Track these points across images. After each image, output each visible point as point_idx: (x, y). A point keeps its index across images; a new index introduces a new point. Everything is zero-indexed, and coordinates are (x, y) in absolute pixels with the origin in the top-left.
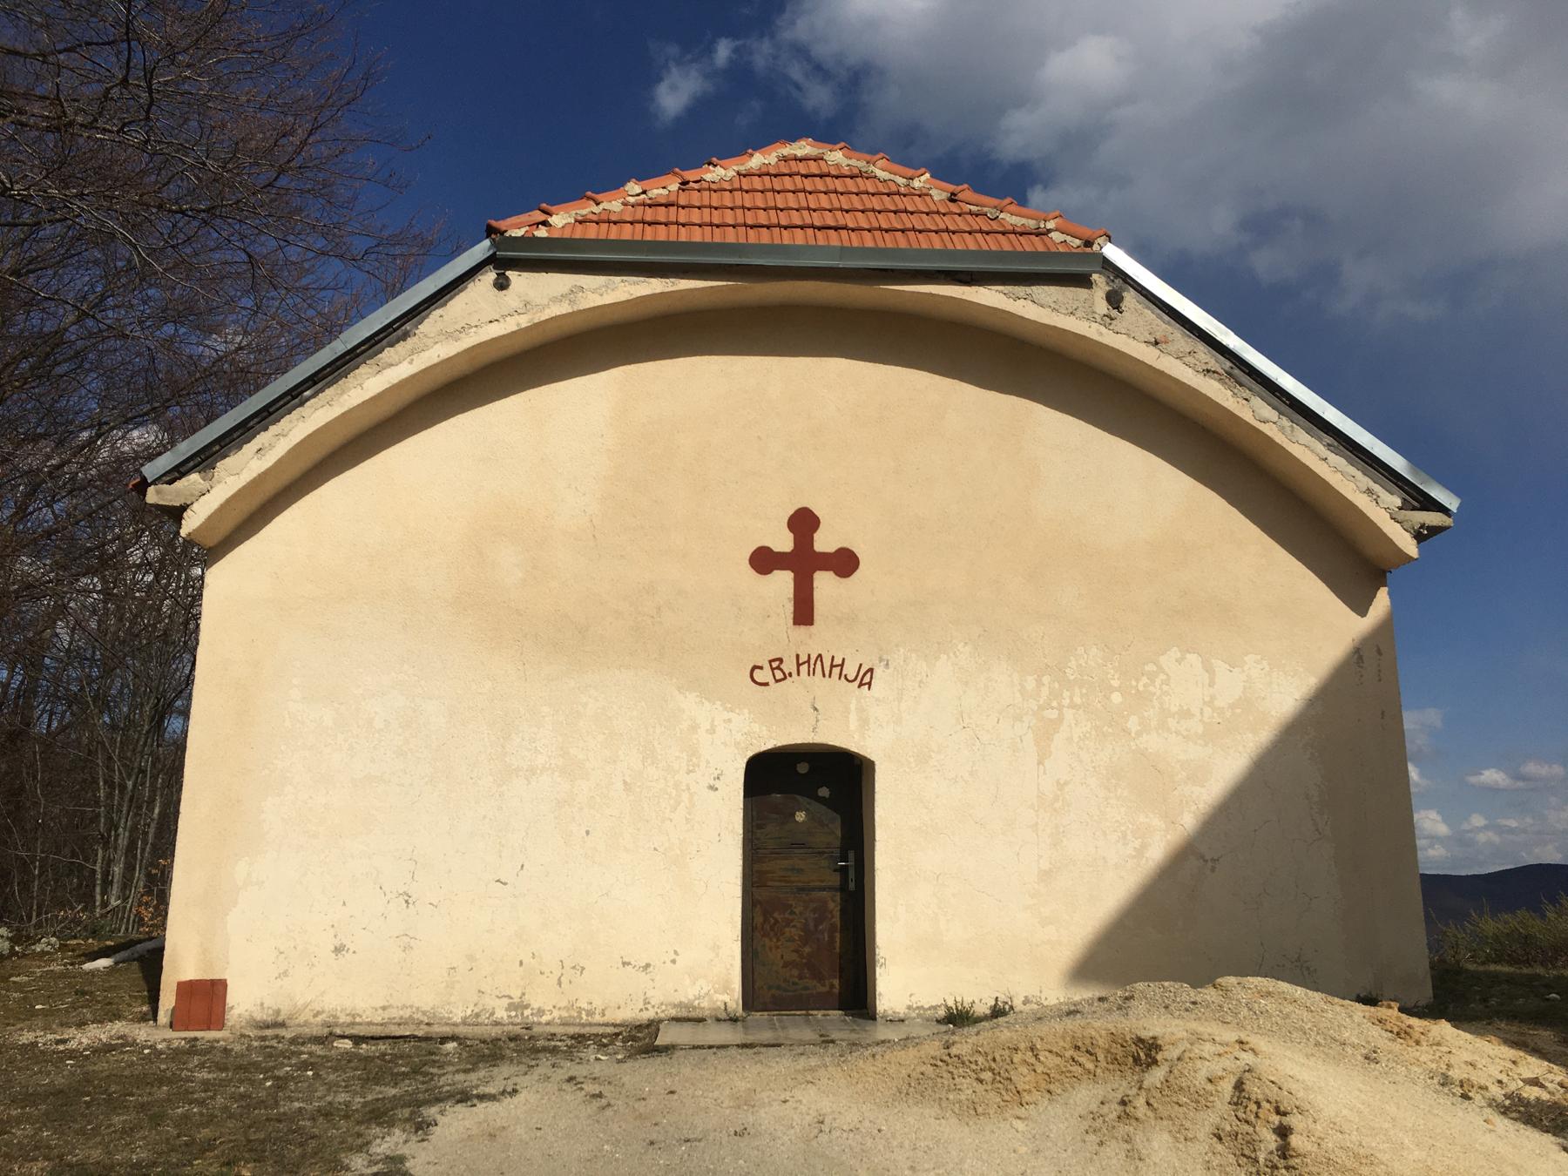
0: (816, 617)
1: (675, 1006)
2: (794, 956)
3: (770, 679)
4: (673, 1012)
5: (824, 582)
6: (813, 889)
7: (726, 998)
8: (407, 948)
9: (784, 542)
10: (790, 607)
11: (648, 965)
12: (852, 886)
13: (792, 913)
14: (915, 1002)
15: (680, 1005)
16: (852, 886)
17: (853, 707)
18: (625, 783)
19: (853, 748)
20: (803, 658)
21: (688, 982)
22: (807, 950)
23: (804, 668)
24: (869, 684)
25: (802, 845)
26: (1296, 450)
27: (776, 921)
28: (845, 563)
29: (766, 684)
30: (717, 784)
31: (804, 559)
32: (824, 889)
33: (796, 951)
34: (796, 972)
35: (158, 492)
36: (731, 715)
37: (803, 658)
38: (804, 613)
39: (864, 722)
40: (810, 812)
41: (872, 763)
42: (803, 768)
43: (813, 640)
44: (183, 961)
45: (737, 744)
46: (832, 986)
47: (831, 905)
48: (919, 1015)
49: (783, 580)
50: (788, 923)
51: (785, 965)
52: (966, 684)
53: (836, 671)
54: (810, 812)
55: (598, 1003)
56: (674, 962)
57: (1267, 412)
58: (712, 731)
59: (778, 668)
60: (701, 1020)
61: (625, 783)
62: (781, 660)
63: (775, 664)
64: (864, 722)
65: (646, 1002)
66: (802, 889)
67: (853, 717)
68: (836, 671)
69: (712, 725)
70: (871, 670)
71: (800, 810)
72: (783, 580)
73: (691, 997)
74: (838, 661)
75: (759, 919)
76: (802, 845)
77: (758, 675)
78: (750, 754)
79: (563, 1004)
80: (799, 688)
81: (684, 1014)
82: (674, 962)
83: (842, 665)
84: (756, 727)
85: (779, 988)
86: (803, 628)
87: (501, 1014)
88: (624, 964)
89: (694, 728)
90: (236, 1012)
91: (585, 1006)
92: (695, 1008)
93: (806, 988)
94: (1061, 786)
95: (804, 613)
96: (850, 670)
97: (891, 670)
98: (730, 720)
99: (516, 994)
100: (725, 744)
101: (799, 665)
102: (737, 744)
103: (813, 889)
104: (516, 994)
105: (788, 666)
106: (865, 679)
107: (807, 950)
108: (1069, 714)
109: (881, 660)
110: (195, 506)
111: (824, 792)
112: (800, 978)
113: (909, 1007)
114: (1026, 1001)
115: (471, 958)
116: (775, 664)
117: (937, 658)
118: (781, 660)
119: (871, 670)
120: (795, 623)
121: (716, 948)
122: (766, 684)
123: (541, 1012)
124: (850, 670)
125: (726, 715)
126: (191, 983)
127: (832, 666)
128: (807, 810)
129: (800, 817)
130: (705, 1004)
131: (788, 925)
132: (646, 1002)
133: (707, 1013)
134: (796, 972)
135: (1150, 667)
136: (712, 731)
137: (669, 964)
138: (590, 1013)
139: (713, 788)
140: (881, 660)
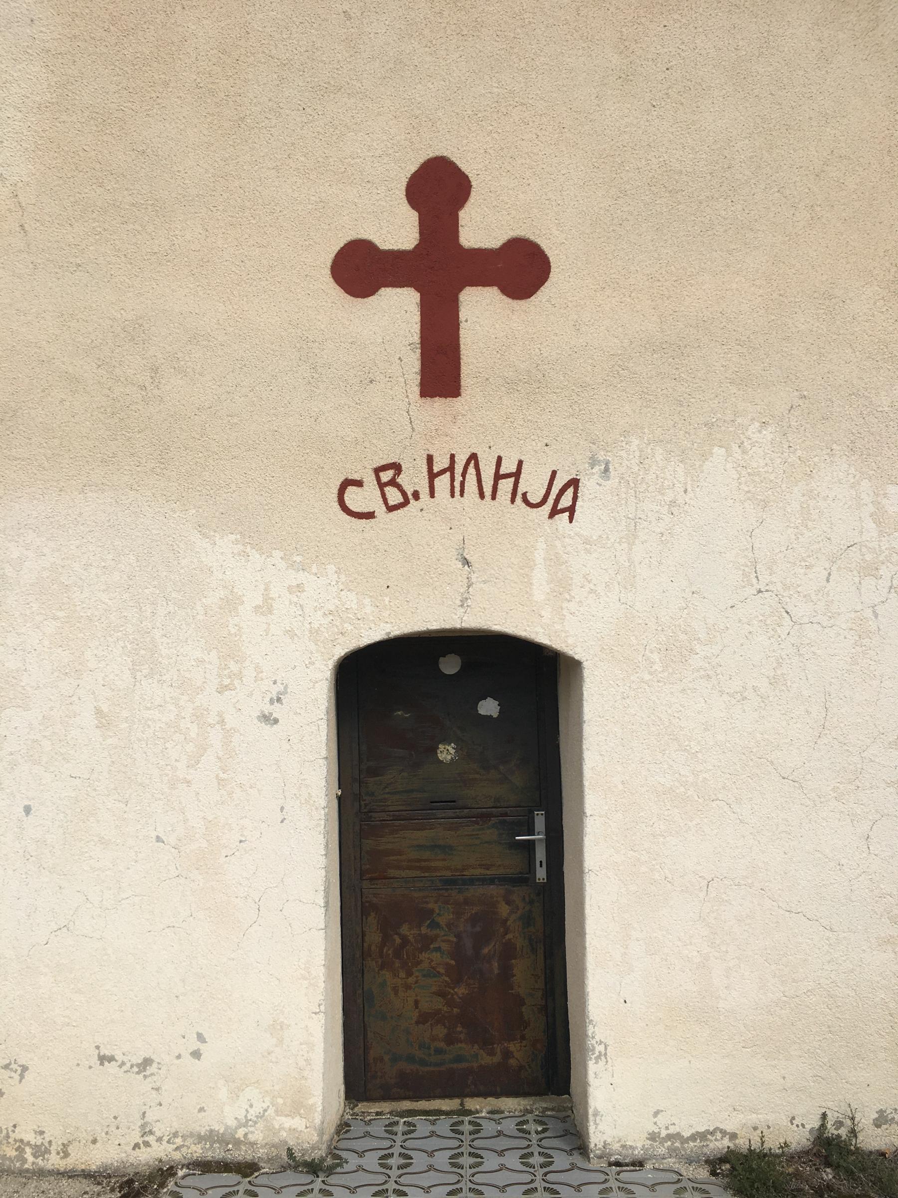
0: (462, 390)
1: (200, 1138)
2: (438, 1004)
3: (379, 508)
4: (197, 1151)
5: (481, 311)
6: (472, 881)
7: (298, 1123)
9: (399, 230)
10: (413, 362)
11: (147, 1062)
12: (541, 874)
13: (434, 925)
14: (666, 1124)
15: (211, 1137)
16: (541, 874)
17: (539, 556)
18: (98, 712)
19: (542, 639)
20: (440, 463)
21: (223, 1093)
22: (461, 991)
23: (442, 483)
24: (571, 510)
25: (450, 803)
27: (405, 941)
28: (521, 269)
29: (370, 515)
30: (277, 711)
31: (441, 262)
32: (492, 881)
33: (441, 994)
34: (440, 1031)
36: (302, 577)
37: (440, 463)
38: (440, 372)
39: (561, 587)
40: (455, 755)
41: (575, 666)
42: (450, 666)
43: (470, 424)
45: (315, 633)
46: (507, 1054)
47: (504, 910)
48: (672, 1152)
49: (398, 311)
50: (426, 943)
51: (423, 1019)
52: (765, 505)
53: (506, 485)
54: (455, 755)
55: (55, 1134)
56: (196, 1054)
58: (265, 608)
59: (393, 483)
60: (247, 1169)
61: (98, 712)
62: (397, 468)
63: (386, 476)
64: (561, 587)
65: (146, 1131)
66: (450, 882)
67: (540, 575)
68: (506, 485)
69: (267, 598)
70: (574, 483)
71: (446, 741)
72: (398, 311)
73: (232, 1123)
74: (508, 467)
75: (374, 937)
76: (450, 803)
77: (353, 497)
78: (341, 651)
80: (437, 521)
81: (216, 1153)
82: (196, 1054)
83: (517, 475)
84: (351, 600)
85: (411, 1059)
86: (439, 402)
89: (231, 603)
91: (30, 1137)
92: (237, 1143)
93: (459, 1059)
95: (440, 372)
96: (533, 484)
97: (613, 482)
98: (300, 587)
100: (290, 633)
101: (432, 476)
102: (315, 633)
103: (472, 881)
105: (413, 478)
106: (562, 499)
107: (461, 991)
109: (593, 462)
111: (489, 707)
112: (450, 1040)
113: (653, 1137)
114: (881, 1120)
116: (386, 476)
117: (705, 456)
118: (397, 468)
119: (574, 483)
120: (424, 394)
122: (370, 515)
124: (533, 484)
125: (294, 578)
126: (423, 385)
127: (498, 477)
128: (458, 741)
129: (446, 753)
130: (257, 1135)
131: (425, 948)
132: (146, 1131)
133: (261, 1152)
134: (440, 1031)
136: (265, 608)
137: (187, 1059)
138: (40, 1151)
139: (268, 719)
140: (593, 462)
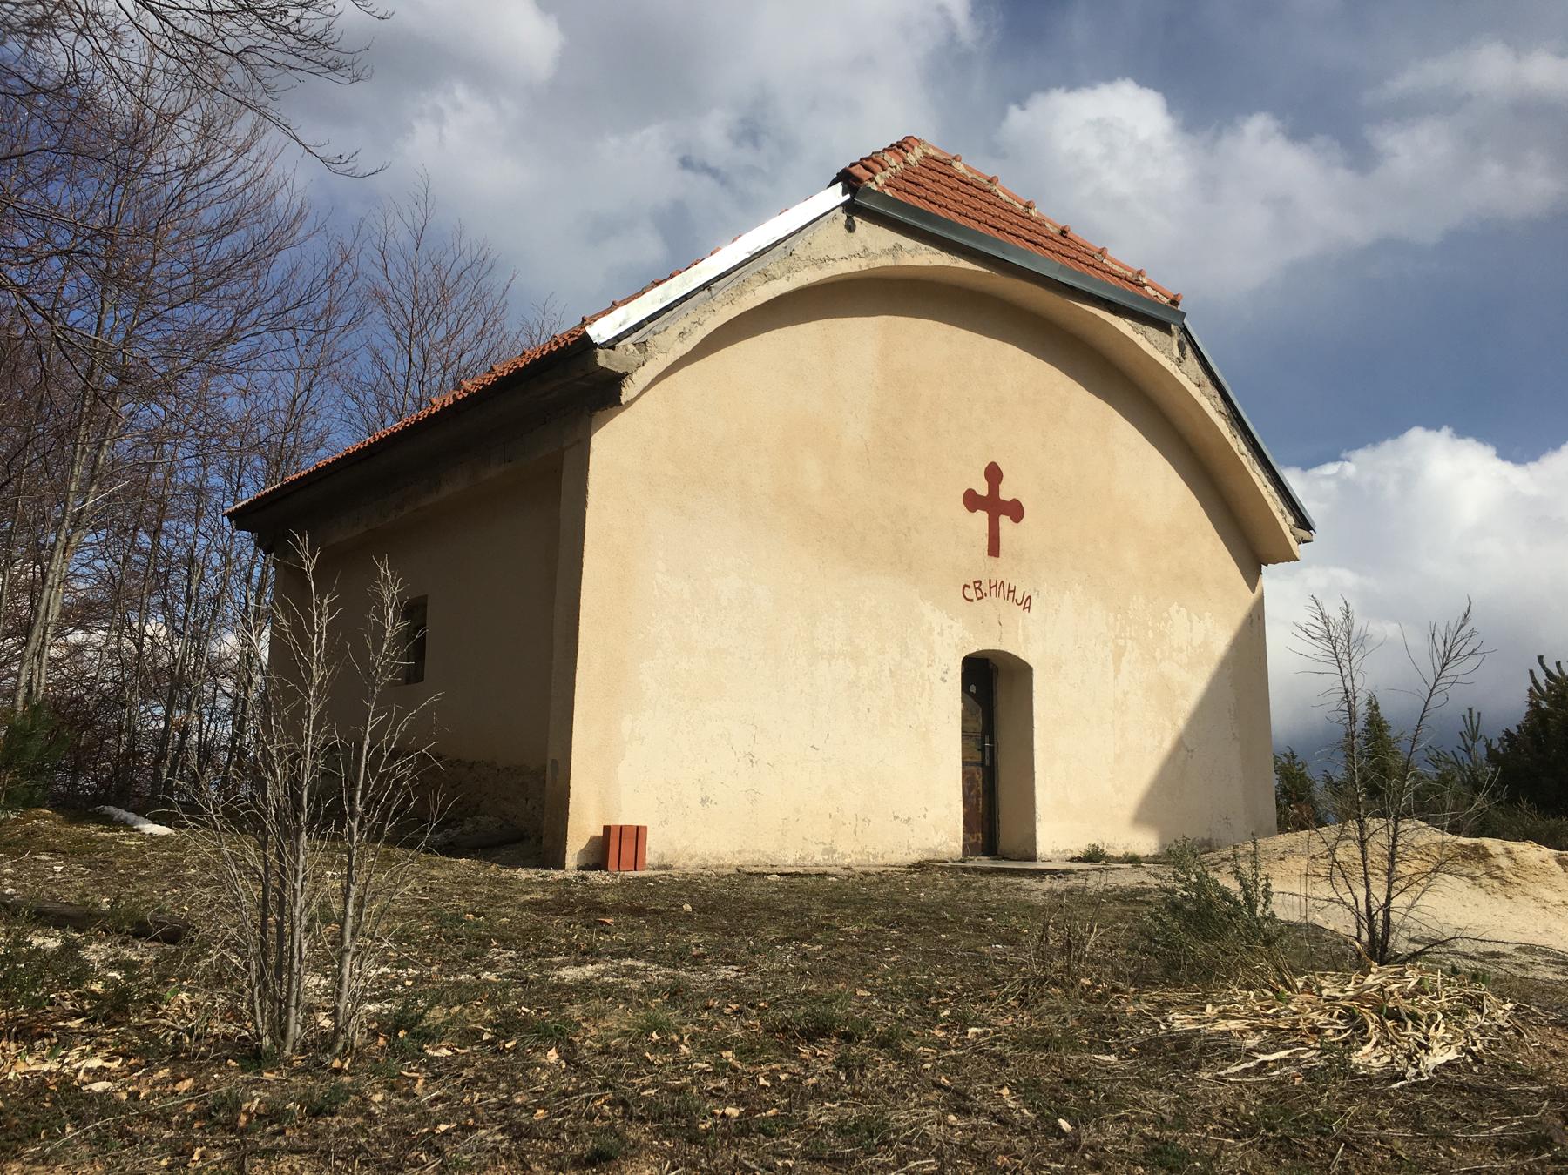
8: (754, 801)
15: (929, 850)
26: (1254, 476)
35: (607, 356)
38: (994, 549)
43: (999, 570)
44: (584, 824)
55: (879, 848)
57: (1244, 448)
58: (941, 634)
63: (970, 593)
79: (858, 849)
80: (993, 606)
87: (819, 858)
88: (896, 818)
90: (282, 198)
94: (1125, 694)
96: (1019, 597)
99: (828, 841)
104: (828, 841)
108: (1130, 643)
110: (634, 377)
115: (797, 810)
121: (949, 805)
123: (844, 856)
124: (1019, 597)
135: (1165, 615)
136: (941, 634)
138: (875, 857)
